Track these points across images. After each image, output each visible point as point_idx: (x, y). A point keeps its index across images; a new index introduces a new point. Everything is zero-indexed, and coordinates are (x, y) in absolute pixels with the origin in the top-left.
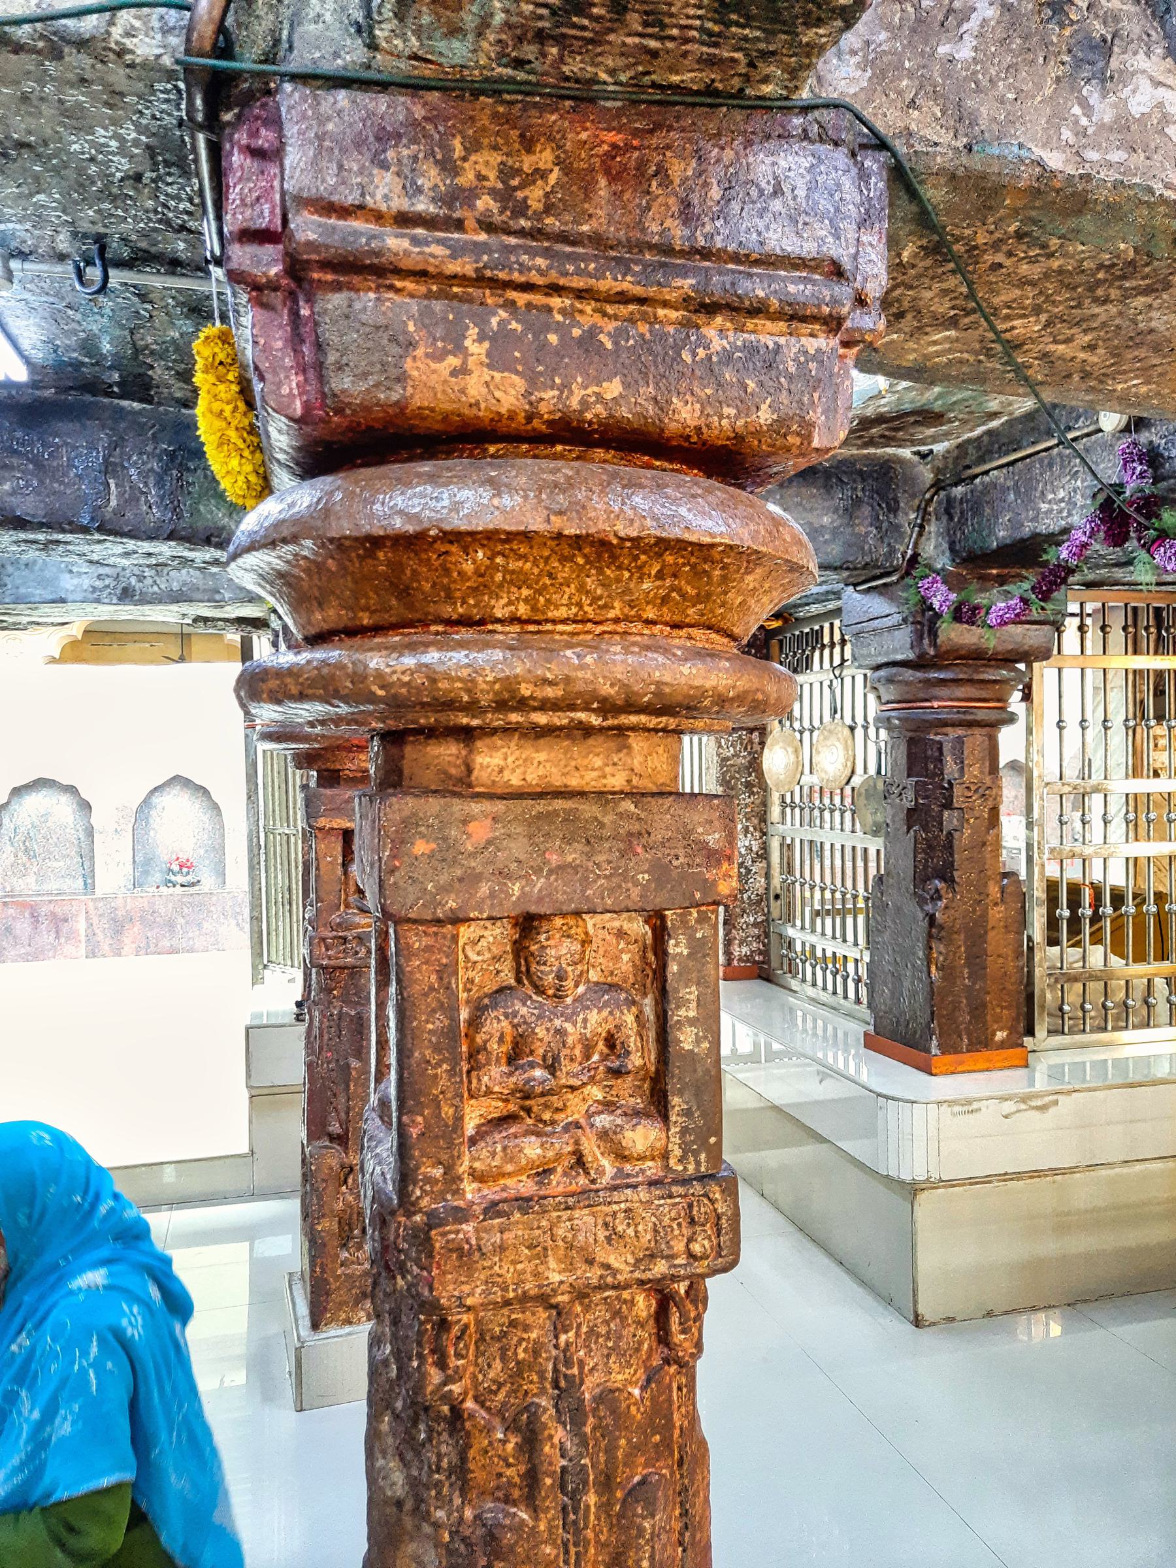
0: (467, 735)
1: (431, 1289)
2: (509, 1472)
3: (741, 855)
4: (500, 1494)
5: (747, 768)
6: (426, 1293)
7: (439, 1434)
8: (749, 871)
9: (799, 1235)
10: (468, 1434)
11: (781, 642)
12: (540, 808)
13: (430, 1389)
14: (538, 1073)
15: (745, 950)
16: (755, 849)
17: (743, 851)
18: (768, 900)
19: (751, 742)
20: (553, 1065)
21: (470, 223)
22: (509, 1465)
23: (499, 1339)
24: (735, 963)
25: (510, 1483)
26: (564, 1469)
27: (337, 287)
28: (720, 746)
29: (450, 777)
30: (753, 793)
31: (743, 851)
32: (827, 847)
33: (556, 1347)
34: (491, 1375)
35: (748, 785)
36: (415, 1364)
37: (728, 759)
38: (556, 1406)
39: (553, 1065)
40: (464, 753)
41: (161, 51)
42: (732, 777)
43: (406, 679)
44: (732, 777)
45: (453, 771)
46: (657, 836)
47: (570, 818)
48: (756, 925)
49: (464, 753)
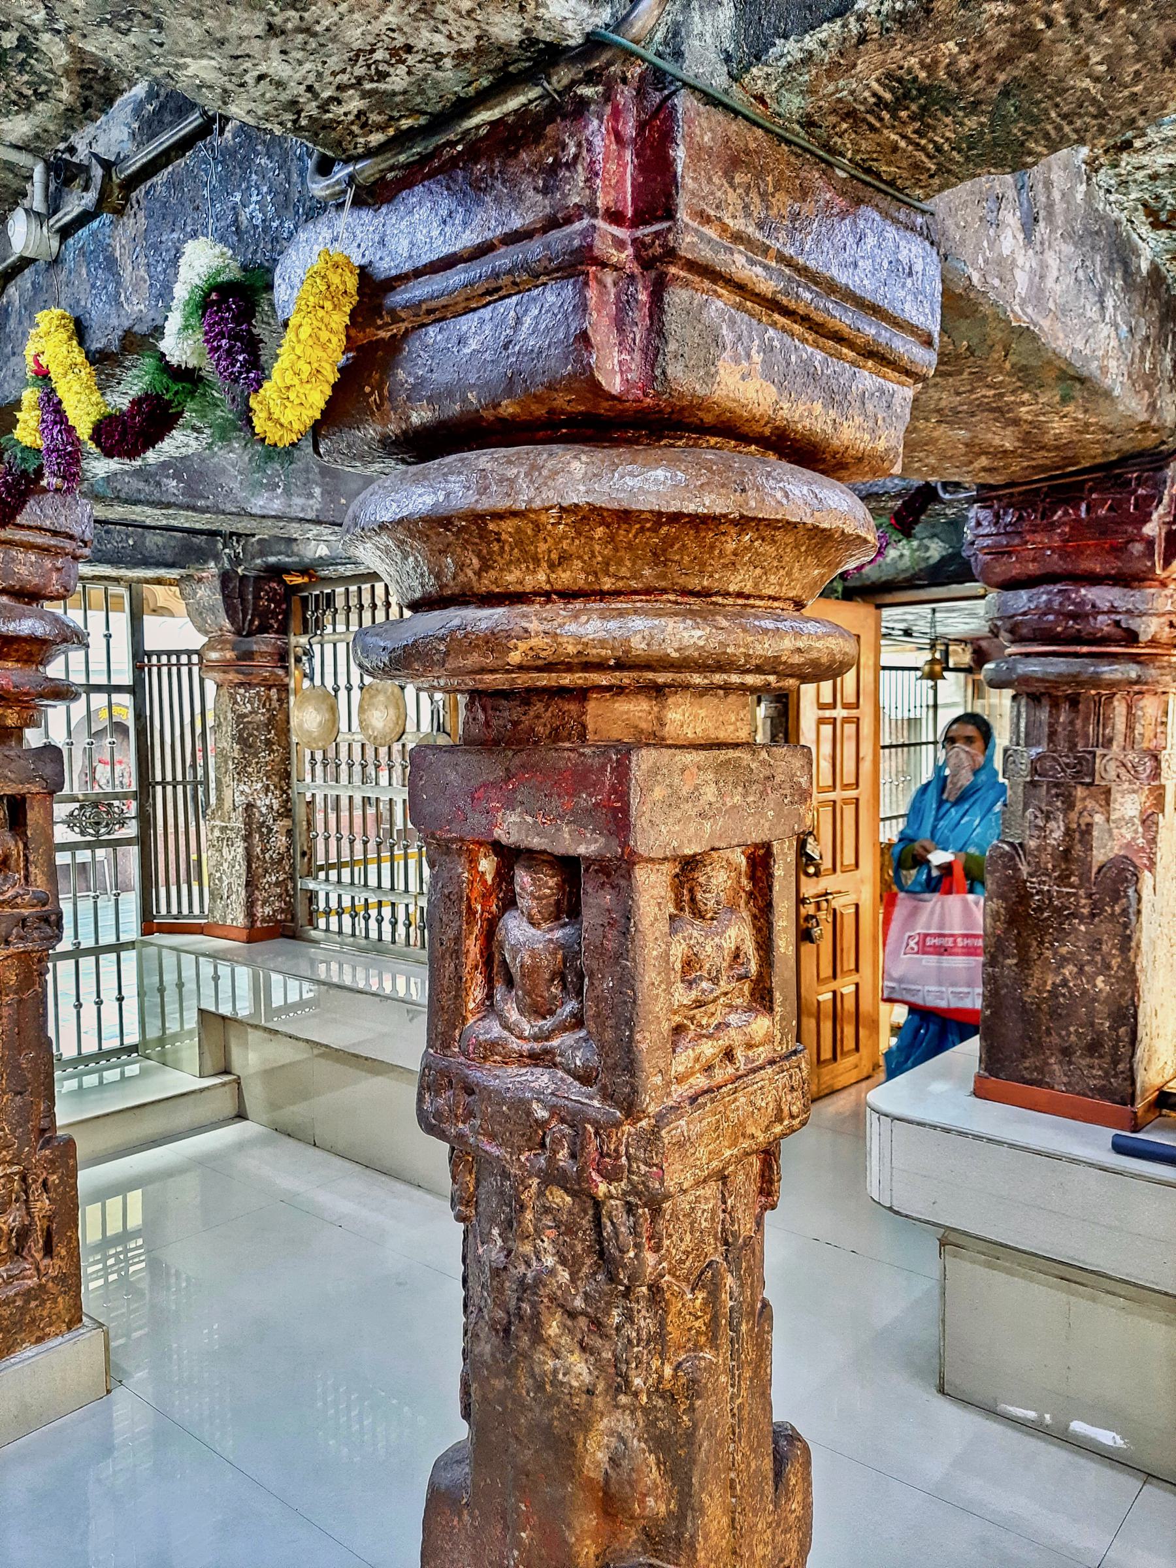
0: (658, 691)
1: (662, 1183)
2: (697, 1324)
3: (262, 815)
4: (690, 1345)
5: (267, 725)
6: (657, 1186)
7: (639, 1311)
8: (270, 830)
9: (368, 1171)
10: (667, 1302)
11: (305, 600)
12: (722, 758)
13: (649, 1270)
14: (705, 985)
15: (268, 910)
16: (275, 807)
17: (264, 810)
18: (291, 857)
19: (269, 698)
20: (716, 977)
21: (772, 253)
22: (697, 1318)
23: (689, 1215)
24: (258, 924)
25: (698, 1333)
26: (732, 1309)
27: (687, 284)
28: (235, 702)
29: (642, 732)
30: (272, 751)
31: (264, 810)
32: (344, 802)
33: (724, 1211)
34: (683, 1247)
35: (268, 743)
36: (632, 1254)
37: (245, 716)
38: (726, 1258)
39: (716, 977)
40: (656, 709)
41: (569, 15)
42: (250, 735)
43: (701, 643)
44: (250, 735)
45: (643, 725)
46: (778, 780)
47: (736, 765)
48: (278, 884)
49: (656, 709)
